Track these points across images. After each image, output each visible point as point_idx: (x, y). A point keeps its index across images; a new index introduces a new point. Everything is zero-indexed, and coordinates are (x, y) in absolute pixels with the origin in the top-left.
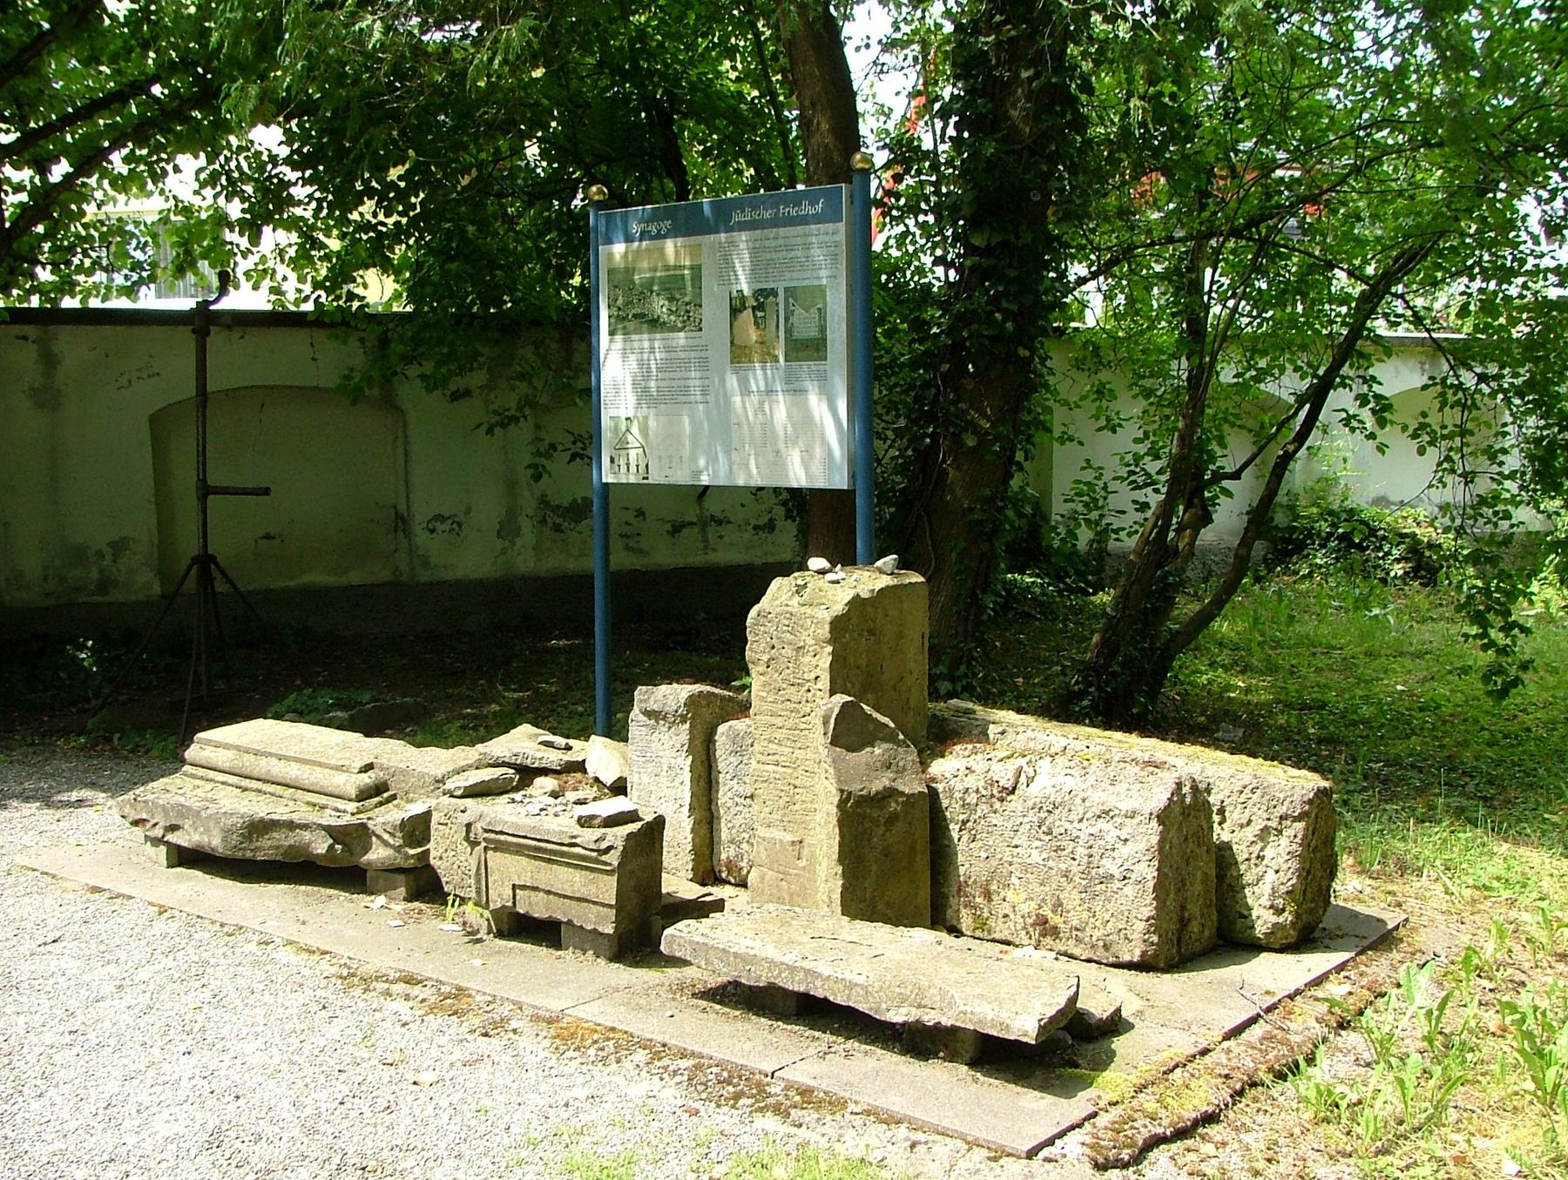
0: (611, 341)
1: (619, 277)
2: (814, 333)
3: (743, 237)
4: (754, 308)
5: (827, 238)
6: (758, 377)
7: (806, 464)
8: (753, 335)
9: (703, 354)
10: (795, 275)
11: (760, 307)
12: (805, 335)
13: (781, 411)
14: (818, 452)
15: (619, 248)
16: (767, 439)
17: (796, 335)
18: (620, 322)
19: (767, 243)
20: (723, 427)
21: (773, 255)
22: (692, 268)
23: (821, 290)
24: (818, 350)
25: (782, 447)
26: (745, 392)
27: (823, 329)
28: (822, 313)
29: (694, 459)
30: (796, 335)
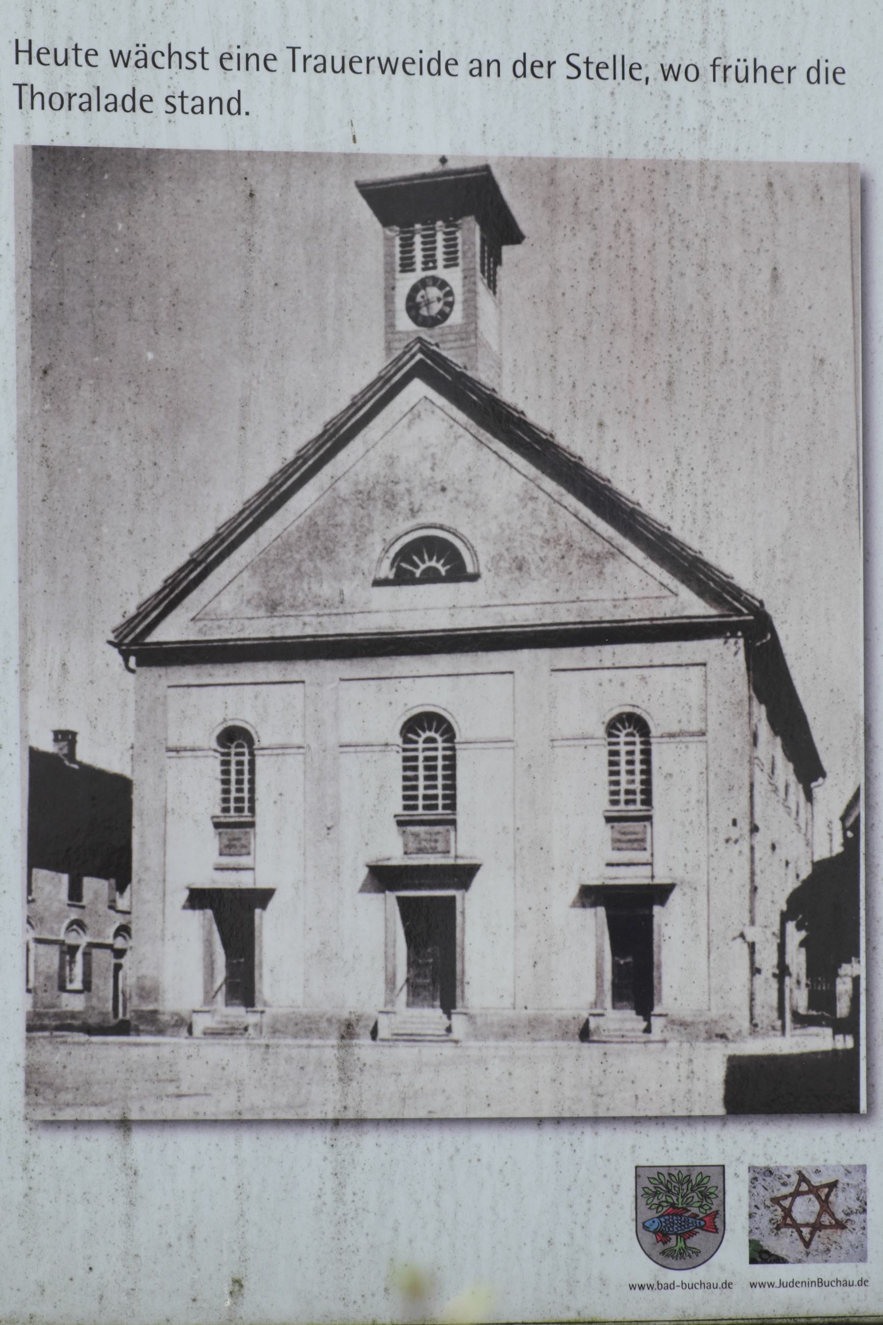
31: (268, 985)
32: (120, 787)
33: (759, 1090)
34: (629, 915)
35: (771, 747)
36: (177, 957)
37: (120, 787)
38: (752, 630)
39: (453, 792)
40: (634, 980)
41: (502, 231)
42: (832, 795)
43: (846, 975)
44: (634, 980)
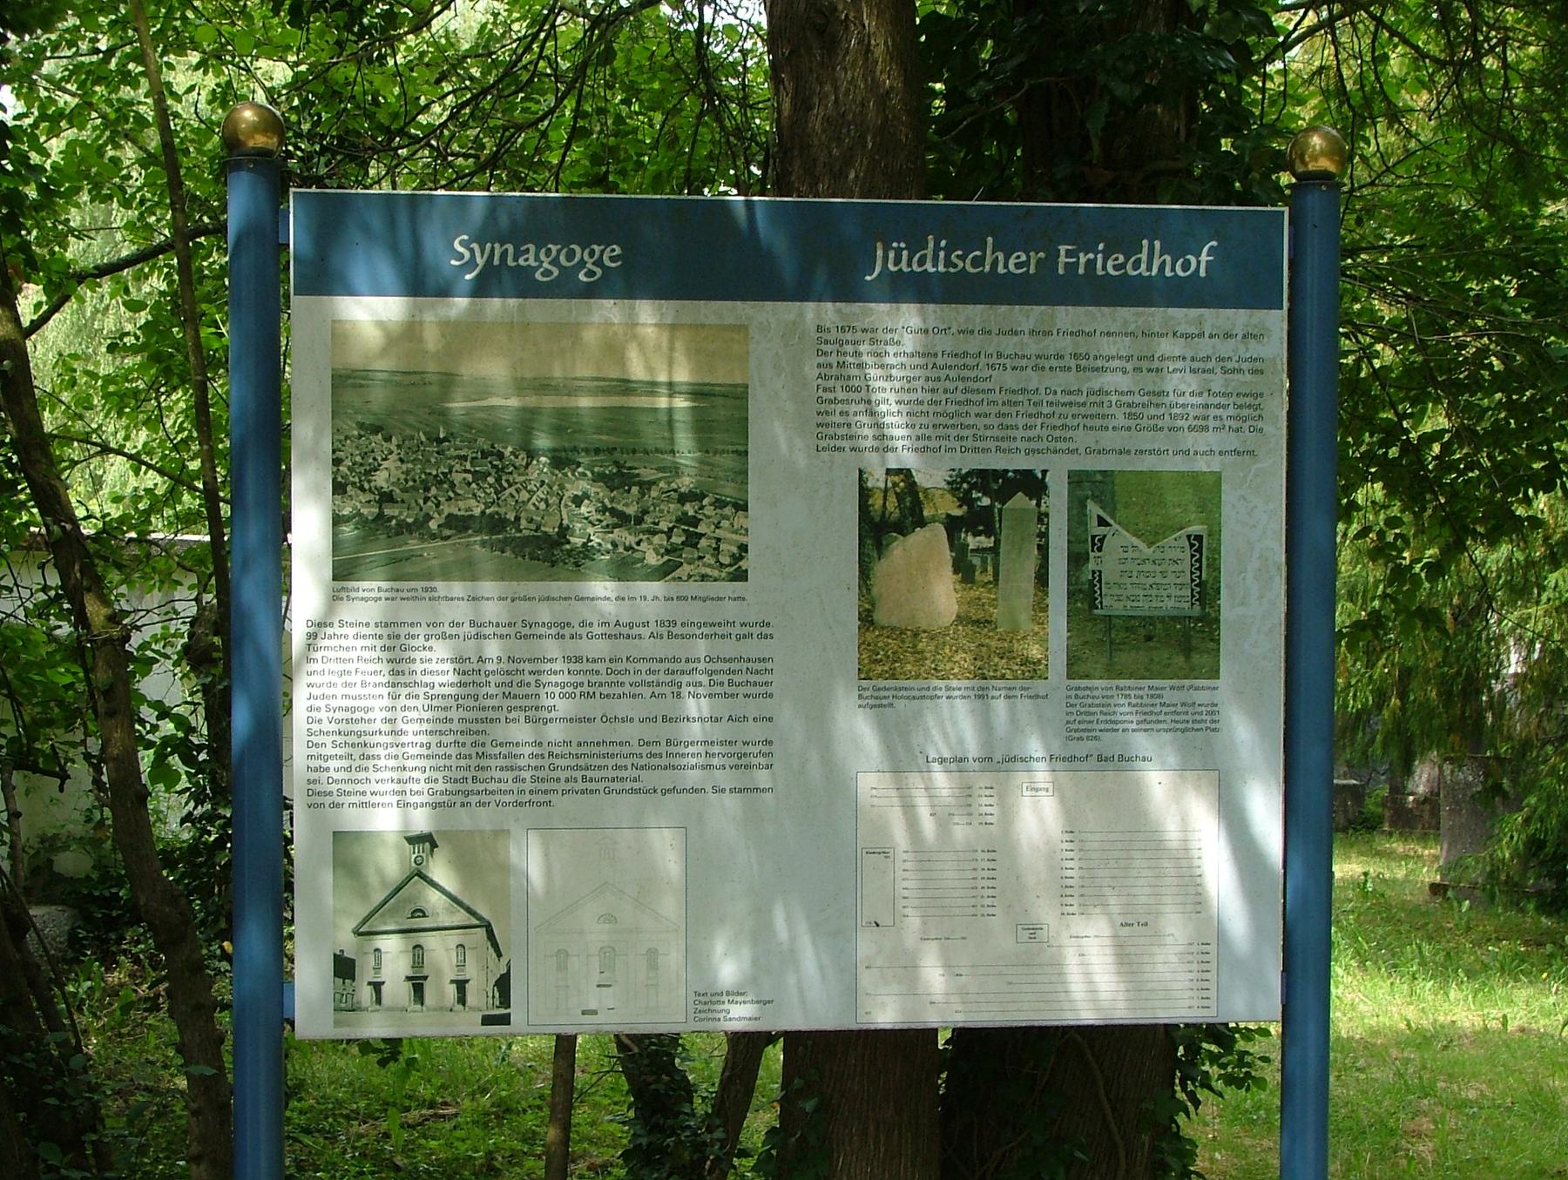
0: (335, 598)
1: (379, 398)
2: (1174, 599)
3: (905, 324)
4: (953, 526)
5: (1226, 348)
6: (953, 717)
7: (1127, 959)
8: (944, 596)
9: (752, 648)
10: (1109, 439)
11: (981, 521)
12: (1144, 607)
13: (1038, 812)
14: (1175, 928)
15: (370, 313)
16: (983, 883)
17: (1112, 603)
18: (381, 537)
19: (1009, 345)
20: (825, 859)
21: (1033, 380)
22: (699, 393)
23: (1206, 491)
24: (1187, 650)
25: (1046, 913)
26: (902, 758)
27: (1206, 592)
28: (1203, 549)
29: (697, 958)
30: (1112, 603)
31: (384, 1001)
32: (353, 961)
33: (488, 1020)
34: (461, 985)
35: (491, 951)
36: (366, 994)
37: (353, 961)
38: (489, 928)
39: (788, 268)
40: (462, 1000)
41: (434, 845)
42: (504, 961)
43: (934, 520)
44: (462, 1000)
